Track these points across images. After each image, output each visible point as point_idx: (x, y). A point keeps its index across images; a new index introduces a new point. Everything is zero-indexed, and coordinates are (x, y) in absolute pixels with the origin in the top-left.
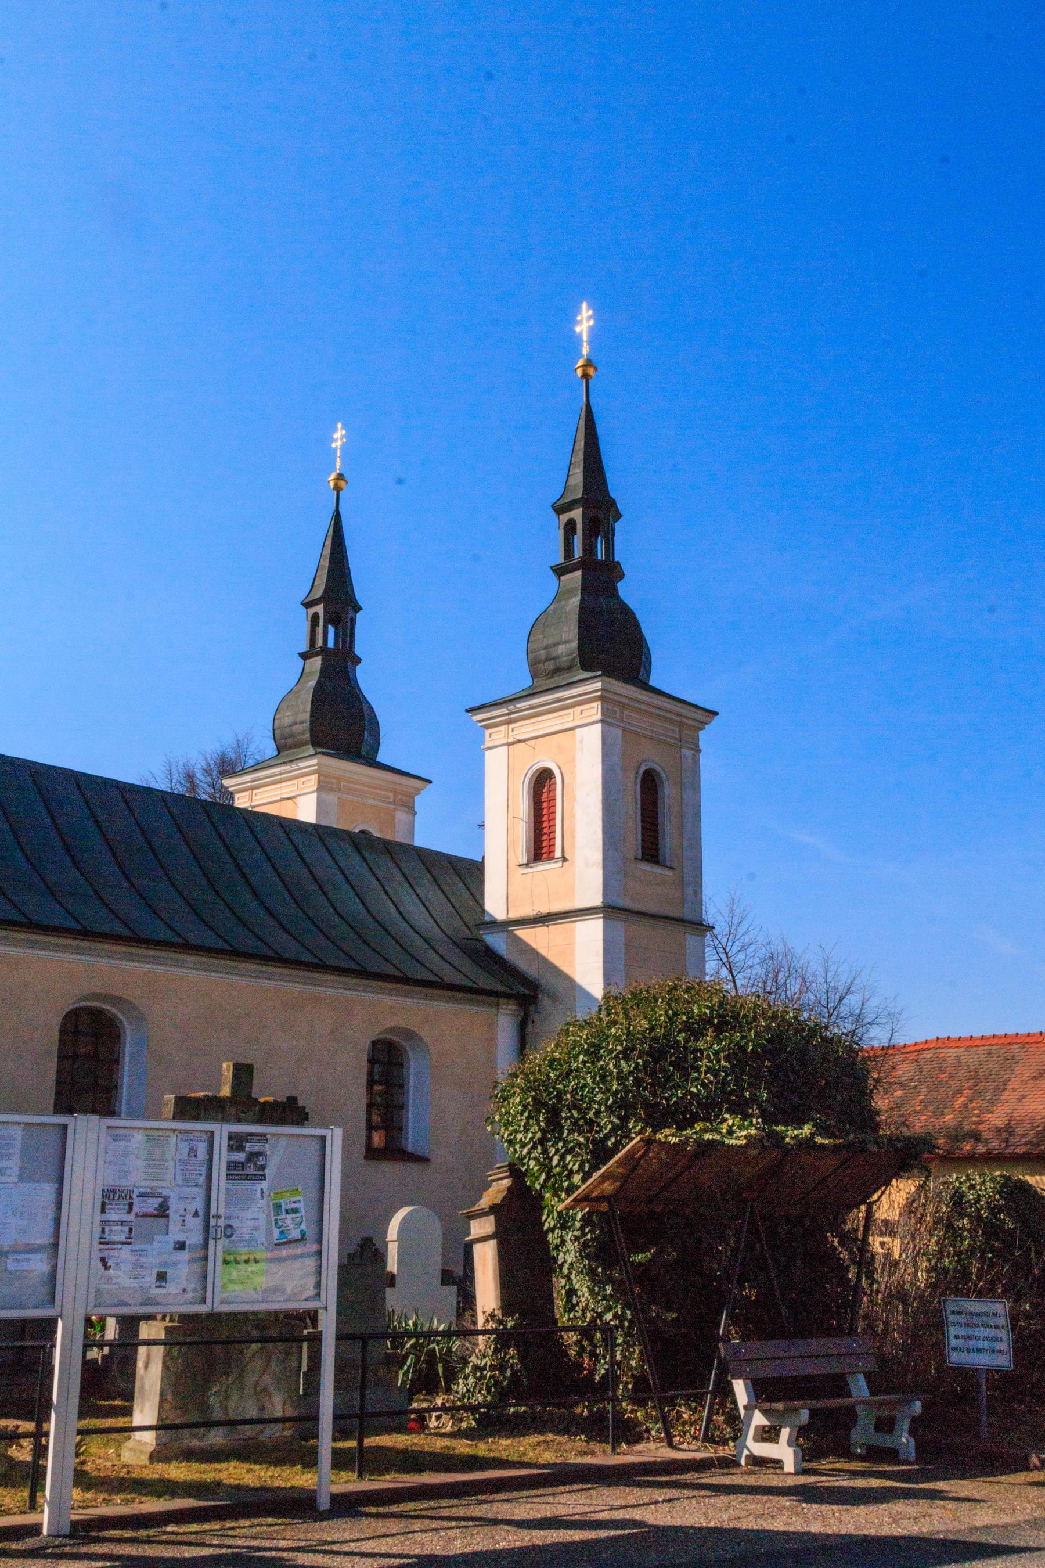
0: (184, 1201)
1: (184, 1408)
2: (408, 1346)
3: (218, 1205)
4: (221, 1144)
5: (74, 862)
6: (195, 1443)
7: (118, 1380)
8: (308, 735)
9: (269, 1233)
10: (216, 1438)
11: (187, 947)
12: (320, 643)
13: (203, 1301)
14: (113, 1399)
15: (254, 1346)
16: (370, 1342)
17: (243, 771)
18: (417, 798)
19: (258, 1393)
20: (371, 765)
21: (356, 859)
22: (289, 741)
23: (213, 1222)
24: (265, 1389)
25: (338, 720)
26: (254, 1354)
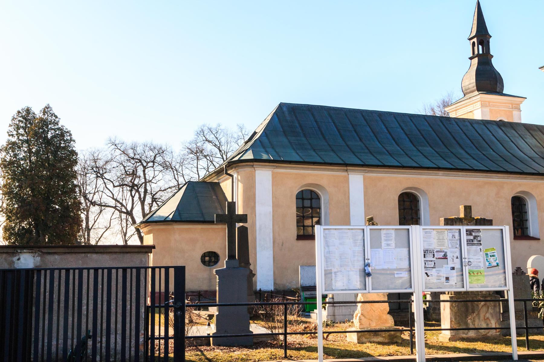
0: (453, 253)
1: (459, 323)
2: (541, 305)
3: (465, 254)
4: (463, 233)
5: (396, 143)
6: (464, 336)
7: (433, 315)
8: (475, 88)
9: (485, 264)
10: (472, 334)
11: (439, 168)
12: (476, 52)
13: (463, 287)
14: (432, 321)
15: (483, 303)
16: (527, 302)
17: (452, 105)
18: (521, 105)
19: (486, 318)
20: (501, 95)
21: (500, 131)
22: (468, 91)
23: (463, 260)
24: (488, 318)
25: (488, 80)
26: (483, 306)
